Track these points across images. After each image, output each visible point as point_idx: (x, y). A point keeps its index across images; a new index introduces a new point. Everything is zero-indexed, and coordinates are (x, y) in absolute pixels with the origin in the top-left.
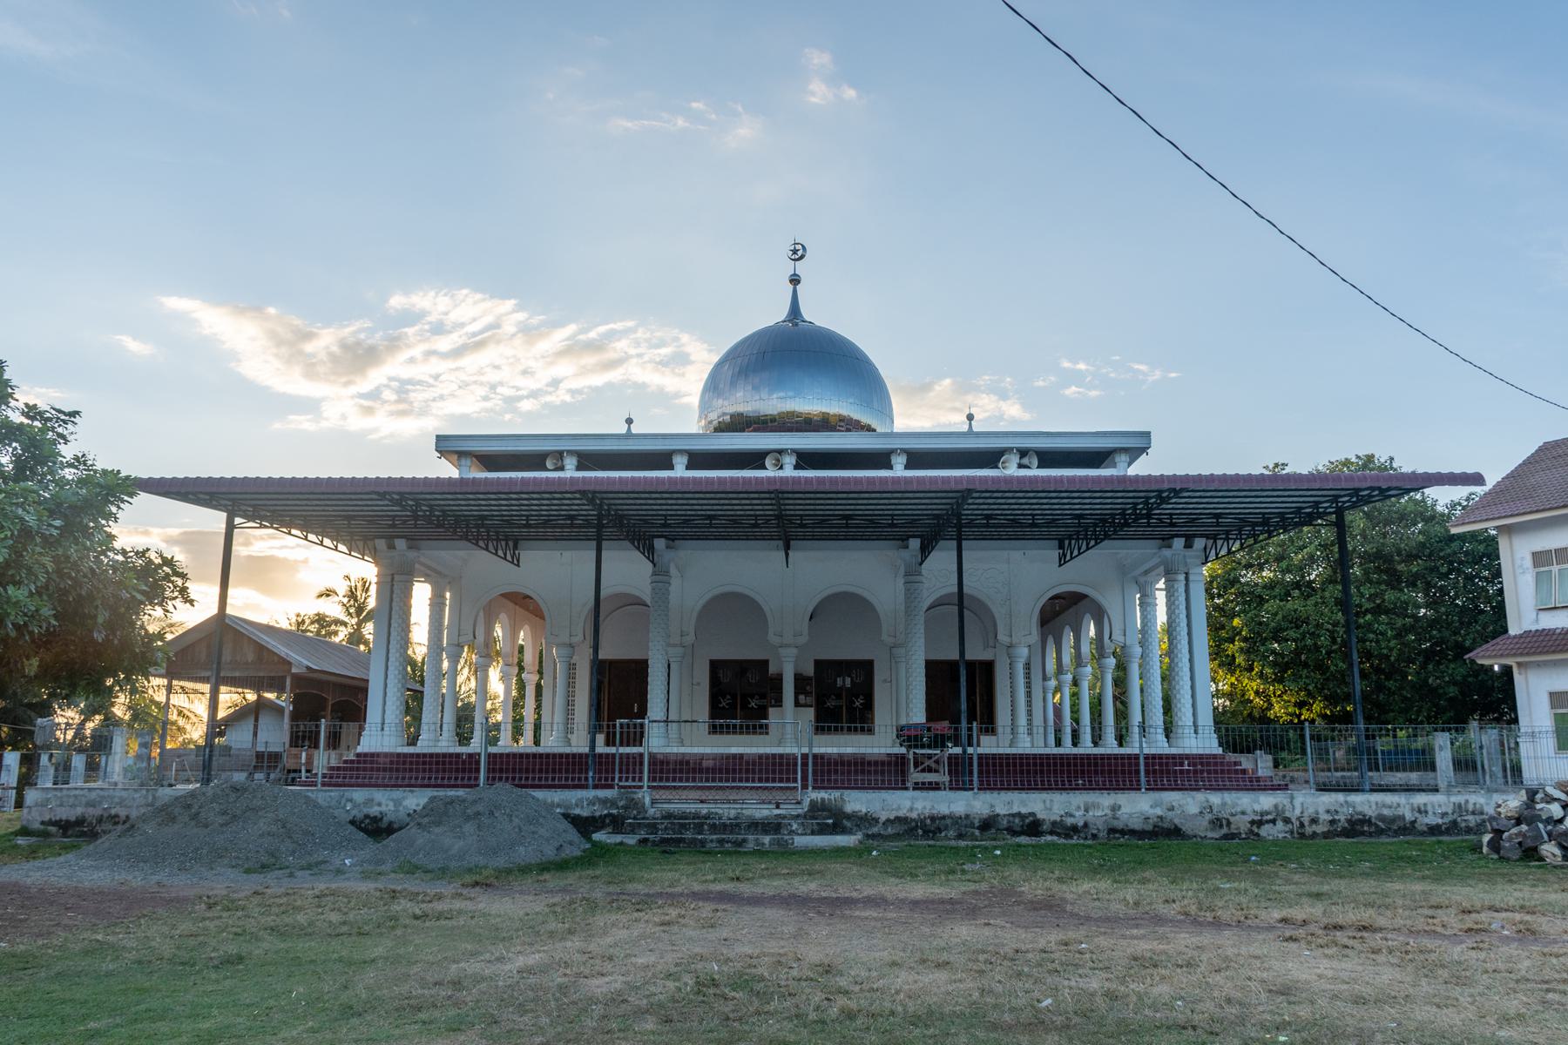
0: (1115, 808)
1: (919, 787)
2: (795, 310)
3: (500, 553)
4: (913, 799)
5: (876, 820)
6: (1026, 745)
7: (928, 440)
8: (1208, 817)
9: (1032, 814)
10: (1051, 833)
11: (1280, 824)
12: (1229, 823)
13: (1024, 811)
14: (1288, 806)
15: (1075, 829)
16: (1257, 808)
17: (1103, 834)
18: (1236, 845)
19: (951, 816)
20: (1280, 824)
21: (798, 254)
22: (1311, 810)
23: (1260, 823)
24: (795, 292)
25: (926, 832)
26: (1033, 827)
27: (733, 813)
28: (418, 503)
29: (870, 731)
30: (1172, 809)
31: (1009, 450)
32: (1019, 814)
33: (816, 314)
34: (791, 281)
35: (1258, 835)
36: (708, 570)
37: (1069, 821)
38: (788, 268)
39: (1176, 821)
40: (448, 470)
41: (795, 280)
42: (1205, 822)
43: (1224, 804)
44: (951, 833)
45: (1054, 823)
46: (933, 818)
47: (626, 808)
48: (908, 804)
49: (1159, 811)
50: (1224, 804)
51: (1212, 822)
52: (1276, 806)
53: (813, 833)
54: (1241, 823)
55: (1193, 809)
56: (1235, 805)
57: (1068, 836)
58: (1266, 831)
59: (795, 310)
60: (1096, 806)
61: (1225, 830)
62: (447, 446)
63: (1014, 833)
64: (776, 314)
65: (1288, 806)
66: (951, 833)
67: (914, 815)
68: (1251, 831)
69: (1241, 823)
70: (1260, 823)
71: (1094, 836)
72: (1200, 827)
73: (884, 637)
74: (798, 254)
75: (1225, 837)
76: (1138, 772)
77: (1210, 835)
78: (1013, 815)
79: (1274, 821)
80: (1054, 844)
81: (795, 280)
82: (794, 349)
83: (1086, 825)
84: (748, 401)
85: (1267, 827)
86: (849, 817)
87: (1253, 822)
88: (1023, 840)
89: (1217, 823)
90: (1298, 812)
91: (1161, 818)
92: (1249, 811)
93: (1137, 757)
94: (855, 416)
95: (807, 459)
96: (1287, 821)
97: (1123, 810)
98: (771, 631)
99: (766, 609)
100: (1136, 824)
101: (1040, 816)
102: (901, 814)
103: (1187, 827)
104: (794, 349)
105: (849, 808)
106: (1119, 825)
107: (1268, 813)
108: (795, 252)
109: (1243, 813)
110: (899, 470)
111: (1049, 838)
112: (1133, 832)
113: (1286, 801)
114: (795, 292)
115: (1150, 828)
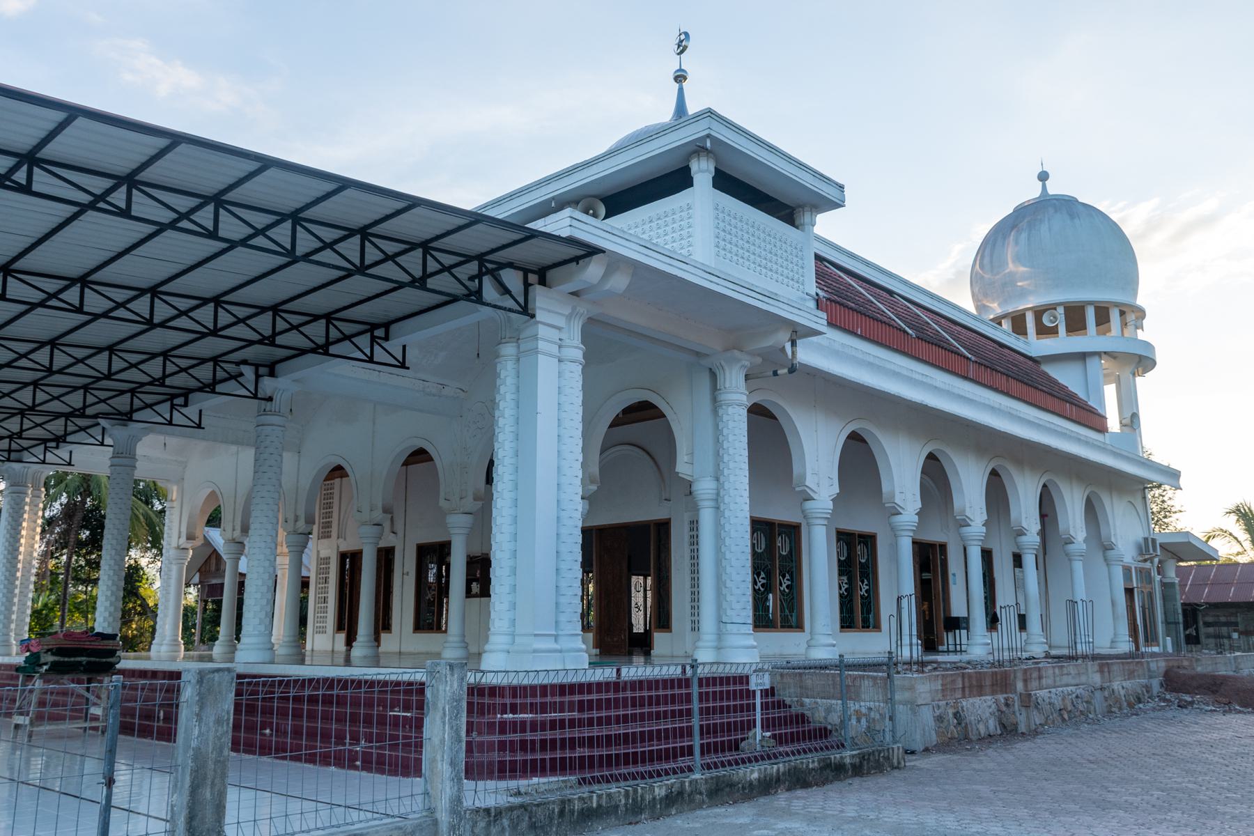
24: (681, 91)
41: (680, 77)
73: (442, 503)
74: (682, 49)
81: (680, 77)
114: (681, 91)
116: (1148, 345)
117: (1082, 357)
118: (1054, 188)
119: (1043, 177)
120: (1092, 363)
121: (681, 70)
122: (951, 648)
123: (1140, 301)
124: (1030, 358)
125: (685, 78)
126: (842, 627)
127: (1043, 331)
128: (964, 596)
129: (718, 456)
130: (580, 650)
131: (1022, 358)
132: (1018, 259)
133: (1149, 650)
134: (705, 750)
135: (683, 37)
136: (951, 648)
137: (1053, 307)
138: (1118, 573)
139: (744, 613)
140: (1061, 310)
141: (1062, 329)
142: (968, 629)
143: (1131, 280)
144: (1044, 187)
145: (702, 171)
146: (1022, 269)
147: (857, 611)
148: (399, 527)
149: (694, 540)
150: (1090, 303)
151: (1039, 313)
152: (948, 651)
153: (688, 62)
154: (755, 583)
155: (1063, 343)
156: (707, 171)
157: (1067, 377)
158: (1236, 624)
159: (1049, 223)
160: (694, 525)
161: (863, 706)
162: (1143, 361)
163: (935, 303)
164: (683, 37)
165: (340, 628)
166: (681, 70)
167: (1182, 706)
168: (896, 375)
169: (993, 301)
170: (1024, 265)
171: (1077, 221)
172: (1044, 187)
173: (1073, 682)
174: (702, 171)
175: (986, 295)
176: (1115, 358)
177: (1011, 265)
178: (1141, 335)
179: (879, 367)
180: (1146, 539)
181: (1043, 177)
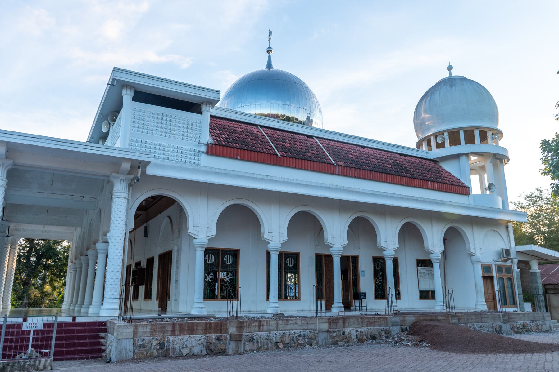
24: (270, 57)
41: (269, 51)
81: (269, 51)
117: (457, 157)
118: (454, 73)
119: (450, 68)
121: (270, 48)
122: (357, 308)
124: (430, 160)
126: (204, 298)
127: (440, 146)
128: (366, 283)
130: (341, 307)
131: (428, 162)
132: (425, 111)
133: (504, 310)
134: (56, 354)
136: (357, 308)
137: (442, 133)
139: (116, 293)
140: (446, 134)
141: (447, 143)
142: (365, 298)
143: (494, 115)
144: (450, 73)
146: (427, 116)
147: (323, 292)
150: (461, 129)
151: (436, 135)
152: (355, 310)
154: (205, 277)
155: (449, 150)
156: (130, 95)
157: (449, 167)
163: (345, 138)
165: (319, 296)
166: (270, 48)
170: (428, 114)
171: (454, 88)
172: (450, 73)
173: (299, 328)
174: (127, 96)
176: (482, 155)
177: (423, 115)
179: (241, 176)
181: (450, 68)
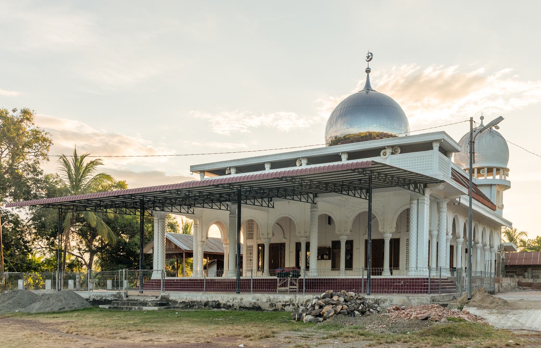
0: (242, 299)
1: (281, 292)
2: (368, 86)
3: (357, 195)
4: (187, 296)
5: (177, 302)
6: (413, 274)
7: (257, 160)
8: (269, 303)
9: (218, 301)
10: (224, 308)
11: (291, 306)
12: (275, 305)
13: (216, 300)
14: (294, 300)
15: (230, 306)
16: (285, 300)
17: (238, 308)
18: (276, 313)
19: (196, 302)
20: (291, 306)
21: (369, 58)
22: (301, 301)
23: (285, 306)
24: (368, 76)
25: (190, 307)
26: (218, 305)
27: (143, 299)
28: (302, 179)
29: (351, 270)
30: (258, 300)
31: (384, 148)
32: (214, 301)
33: (377, 86)
34: (366, 71)
35: (284, 310)
36: (328, 203)
37: (228, 304)
38: (365, 65)
39: (260, 304)
40: (197, 177)
41: (368, 71)
42: (268, 305)
43: (274, 298)
44: (197, 307)
45: (224, 304)
46: (192, 302)
47: (119, 297)
48: (185, 297)
49: (254, 301)
50: (274, 298)
51: (270, 305)
52: (290, 299)
53: (154, 306)
54: (279, 306)
55: (265, 300)
56: (277, 299)
57: (228, 309)
58: (287, 308)
59: (368, 86)
60: (236, 298)
61: (274, 308)
62: (194, 169)
63: (214, 308)
64: (358, 87)
65: (294, 300)
66: (197, 307)
67: (187, 301)
68: (282, 308)
69: (279, 306)
70: (285, 306)
71: (235, 309)
72: (266, 306)
73: (337, 232)
74: (369, 58)
75: (275, 310)
76: (361, 286)
77: (269, 309)
78: (213, 301)
79: (289, 305)
80: (224, 312)
81: (368, 71)
82: (368, 103)
83: (233, 305)
84: (343, 130)
85: (287, 307)
86: (171, 301)
87: (283, 305)
88: (216, 309)
89: (272, 305)
90: (297, 302)
91: (255, 303)
92: (282, 301)
93: (303, 279)
94: (385, 132)
95: (352, 155)
96: (293, 305)
97: (244, 300)
98: (297, 232)
99: (295, 223)
100: (248, 305)
101: (220, 302)
102: (184, 300)
103: (263, 307)
104: (368, 103)
105: (171, 298)
106: (242, 305)
107: (287, 302)
108: (368, 57)
109: (280, 302)
110: (268, 170)
111: (223, 309)
112: (246, 308)
113: (294, 298)
114: (368, 76)
115: (251, 306)
116: (509, 182)
120: (494, 188)
121: (368, 68)
123: (508, 167)
125: (370, 71)
129: (439, 225)
135: (370, 54)
138: (494, 255)
145: (436, 146)
148: (287, 236)
149: (408, 245)
153: (371, 64)
158: (516, 272)
159: (485, 136)
160: (408, 240)
161: (477, 285)
162: (507, 186)
164: (370, 54)
166: (368, 68)
167: (524, 289)
168: (478, 206)
169: (464, 163)
174: (436, 146)
175: (461, 161)
178: (508, 179)
180: (501, 245)
